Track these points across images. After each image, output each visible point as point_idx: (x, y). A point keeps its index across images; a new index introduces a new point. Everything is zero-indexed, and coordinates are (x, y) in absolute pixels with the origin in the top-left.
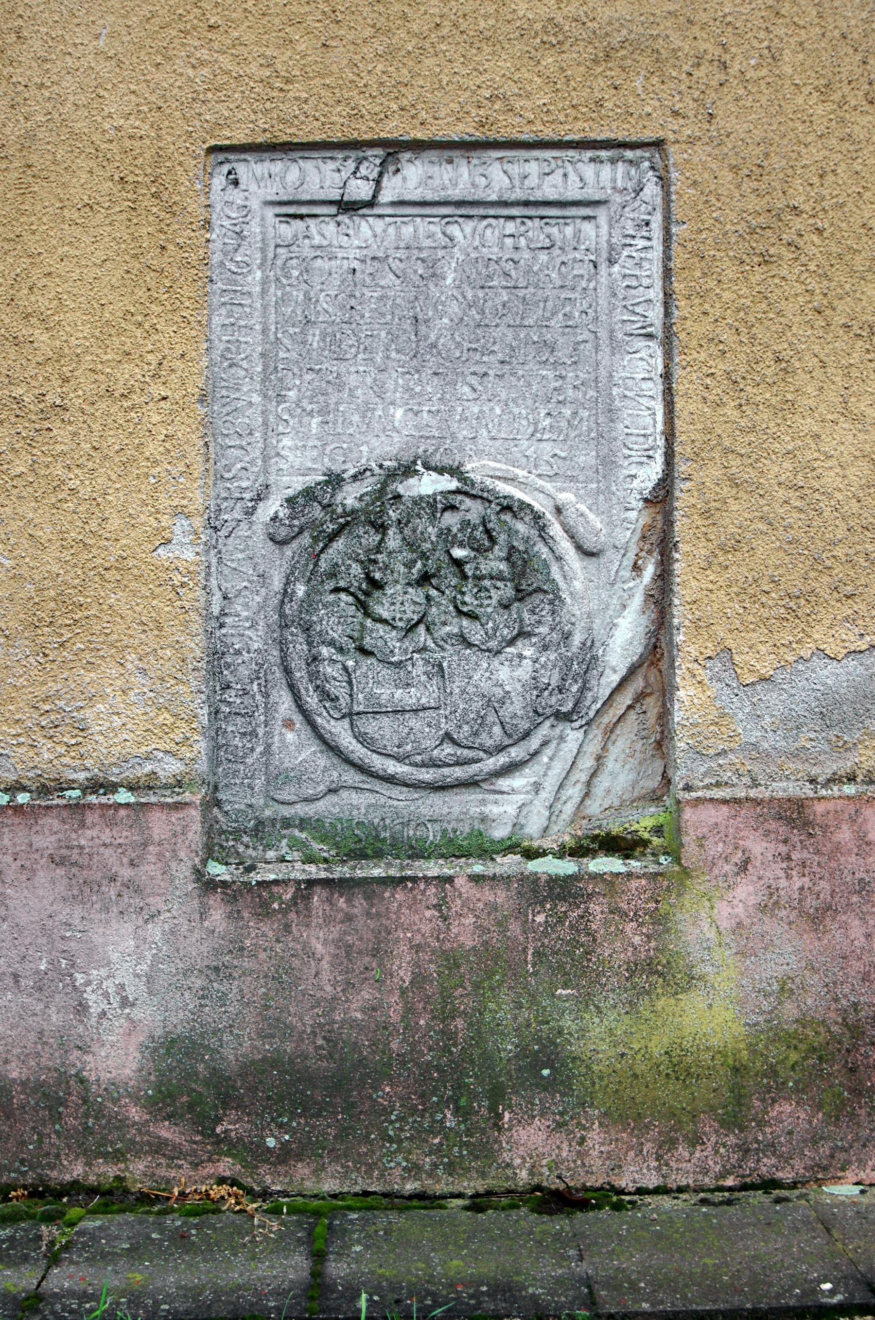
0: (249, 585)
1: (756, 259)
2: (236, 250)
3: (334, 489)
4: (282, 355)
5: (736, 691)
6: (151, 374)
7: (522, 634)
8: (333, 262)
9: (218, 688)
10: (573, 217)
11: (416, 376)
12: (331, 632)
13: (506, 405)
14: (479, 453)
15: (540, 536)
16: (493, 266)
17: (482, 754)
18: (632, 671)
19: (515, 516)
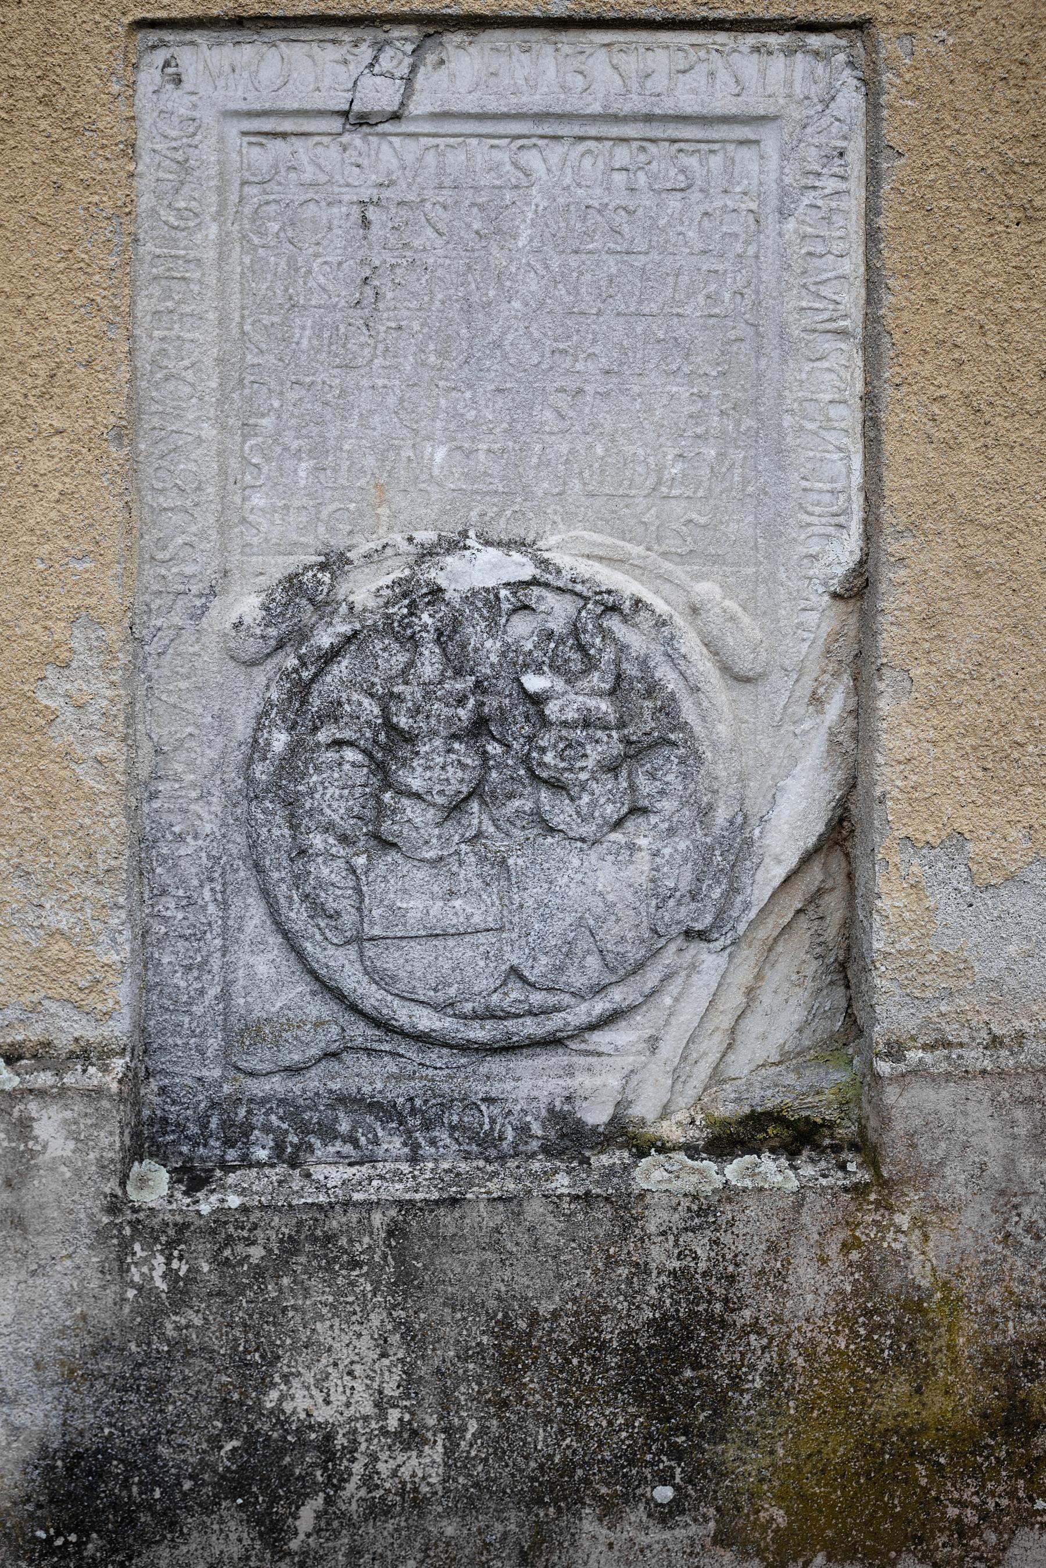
0: (197, 732)
1: (1013, 215)
2: (177, 191)
3: (334, 577)
4: (250, 359)
5: (969, 899)
6: (37, 392)
7: (637, 810)
8: (335, 210)
9: (146, 896)
10: (723, 141)
11: (468, 395)
12: (328, 812)
13: (613, 441)
14: (569, 518)
15: (667, 654)
16: (593, 216)
17: (566, 999)
18: (806, 859)
19: (625, 619)
